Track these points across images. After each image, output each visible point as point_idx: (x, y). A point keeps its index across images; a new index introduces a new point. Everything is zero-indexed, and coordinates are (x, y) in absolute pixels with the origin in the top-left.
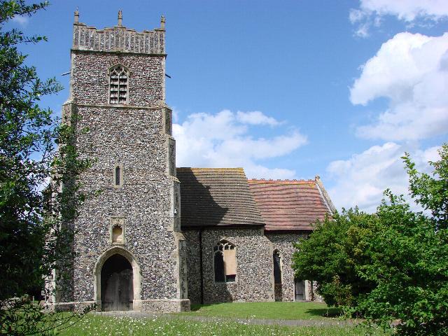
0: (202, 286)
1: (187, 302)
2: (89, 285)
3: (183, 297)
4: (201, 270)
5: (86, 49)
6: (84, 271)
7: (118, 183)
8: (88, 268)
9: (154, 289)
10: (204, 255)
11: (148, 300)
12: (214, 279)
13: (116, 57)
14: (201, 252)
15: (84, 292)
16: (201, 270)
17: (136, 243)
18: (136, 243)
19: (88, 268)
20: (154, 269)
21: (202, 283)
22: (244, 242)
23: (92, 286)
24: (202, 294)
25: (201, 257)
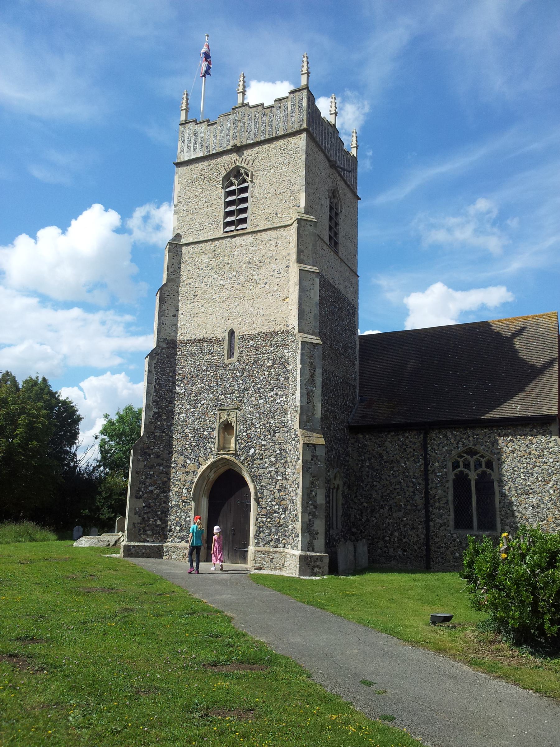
0: (427, 535)
1: (321, 558)
2: (187, 517)
3: (309, 546)
4: (427, 505)
5: (252, 142)
6: (179, 494)
7: (231, 354)
8: (184, 491)
9: (276, 534)
10: (431, 477)
11: (266, 548)
12: (452, 523)
13: (234, 156)
14: (426, 472)
15: (178, 528)
16: (427, 505)
17: (252, 451)
18: (252, 451)
19: (184, 491)
20: (277, 495)
21: (427, 528)
22: (513, 452)
23: (188, 519)
24: (428, 550)
25: (426, 480)
